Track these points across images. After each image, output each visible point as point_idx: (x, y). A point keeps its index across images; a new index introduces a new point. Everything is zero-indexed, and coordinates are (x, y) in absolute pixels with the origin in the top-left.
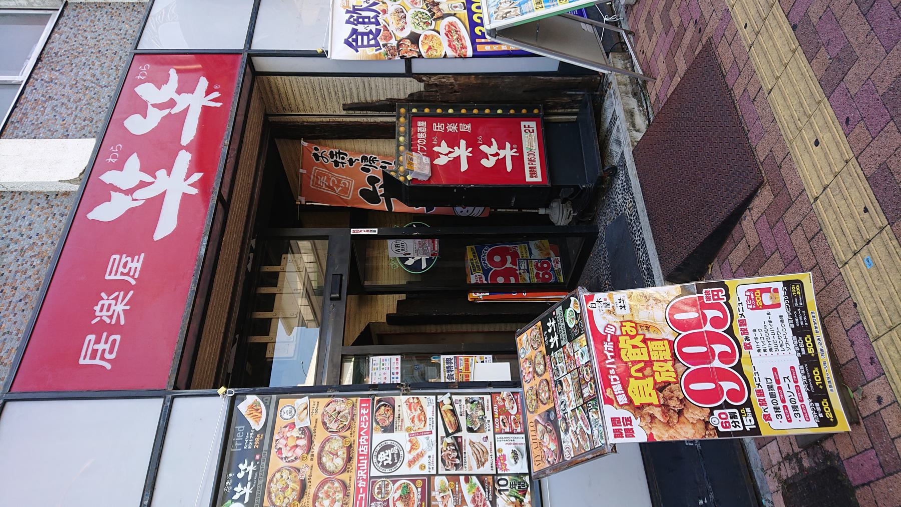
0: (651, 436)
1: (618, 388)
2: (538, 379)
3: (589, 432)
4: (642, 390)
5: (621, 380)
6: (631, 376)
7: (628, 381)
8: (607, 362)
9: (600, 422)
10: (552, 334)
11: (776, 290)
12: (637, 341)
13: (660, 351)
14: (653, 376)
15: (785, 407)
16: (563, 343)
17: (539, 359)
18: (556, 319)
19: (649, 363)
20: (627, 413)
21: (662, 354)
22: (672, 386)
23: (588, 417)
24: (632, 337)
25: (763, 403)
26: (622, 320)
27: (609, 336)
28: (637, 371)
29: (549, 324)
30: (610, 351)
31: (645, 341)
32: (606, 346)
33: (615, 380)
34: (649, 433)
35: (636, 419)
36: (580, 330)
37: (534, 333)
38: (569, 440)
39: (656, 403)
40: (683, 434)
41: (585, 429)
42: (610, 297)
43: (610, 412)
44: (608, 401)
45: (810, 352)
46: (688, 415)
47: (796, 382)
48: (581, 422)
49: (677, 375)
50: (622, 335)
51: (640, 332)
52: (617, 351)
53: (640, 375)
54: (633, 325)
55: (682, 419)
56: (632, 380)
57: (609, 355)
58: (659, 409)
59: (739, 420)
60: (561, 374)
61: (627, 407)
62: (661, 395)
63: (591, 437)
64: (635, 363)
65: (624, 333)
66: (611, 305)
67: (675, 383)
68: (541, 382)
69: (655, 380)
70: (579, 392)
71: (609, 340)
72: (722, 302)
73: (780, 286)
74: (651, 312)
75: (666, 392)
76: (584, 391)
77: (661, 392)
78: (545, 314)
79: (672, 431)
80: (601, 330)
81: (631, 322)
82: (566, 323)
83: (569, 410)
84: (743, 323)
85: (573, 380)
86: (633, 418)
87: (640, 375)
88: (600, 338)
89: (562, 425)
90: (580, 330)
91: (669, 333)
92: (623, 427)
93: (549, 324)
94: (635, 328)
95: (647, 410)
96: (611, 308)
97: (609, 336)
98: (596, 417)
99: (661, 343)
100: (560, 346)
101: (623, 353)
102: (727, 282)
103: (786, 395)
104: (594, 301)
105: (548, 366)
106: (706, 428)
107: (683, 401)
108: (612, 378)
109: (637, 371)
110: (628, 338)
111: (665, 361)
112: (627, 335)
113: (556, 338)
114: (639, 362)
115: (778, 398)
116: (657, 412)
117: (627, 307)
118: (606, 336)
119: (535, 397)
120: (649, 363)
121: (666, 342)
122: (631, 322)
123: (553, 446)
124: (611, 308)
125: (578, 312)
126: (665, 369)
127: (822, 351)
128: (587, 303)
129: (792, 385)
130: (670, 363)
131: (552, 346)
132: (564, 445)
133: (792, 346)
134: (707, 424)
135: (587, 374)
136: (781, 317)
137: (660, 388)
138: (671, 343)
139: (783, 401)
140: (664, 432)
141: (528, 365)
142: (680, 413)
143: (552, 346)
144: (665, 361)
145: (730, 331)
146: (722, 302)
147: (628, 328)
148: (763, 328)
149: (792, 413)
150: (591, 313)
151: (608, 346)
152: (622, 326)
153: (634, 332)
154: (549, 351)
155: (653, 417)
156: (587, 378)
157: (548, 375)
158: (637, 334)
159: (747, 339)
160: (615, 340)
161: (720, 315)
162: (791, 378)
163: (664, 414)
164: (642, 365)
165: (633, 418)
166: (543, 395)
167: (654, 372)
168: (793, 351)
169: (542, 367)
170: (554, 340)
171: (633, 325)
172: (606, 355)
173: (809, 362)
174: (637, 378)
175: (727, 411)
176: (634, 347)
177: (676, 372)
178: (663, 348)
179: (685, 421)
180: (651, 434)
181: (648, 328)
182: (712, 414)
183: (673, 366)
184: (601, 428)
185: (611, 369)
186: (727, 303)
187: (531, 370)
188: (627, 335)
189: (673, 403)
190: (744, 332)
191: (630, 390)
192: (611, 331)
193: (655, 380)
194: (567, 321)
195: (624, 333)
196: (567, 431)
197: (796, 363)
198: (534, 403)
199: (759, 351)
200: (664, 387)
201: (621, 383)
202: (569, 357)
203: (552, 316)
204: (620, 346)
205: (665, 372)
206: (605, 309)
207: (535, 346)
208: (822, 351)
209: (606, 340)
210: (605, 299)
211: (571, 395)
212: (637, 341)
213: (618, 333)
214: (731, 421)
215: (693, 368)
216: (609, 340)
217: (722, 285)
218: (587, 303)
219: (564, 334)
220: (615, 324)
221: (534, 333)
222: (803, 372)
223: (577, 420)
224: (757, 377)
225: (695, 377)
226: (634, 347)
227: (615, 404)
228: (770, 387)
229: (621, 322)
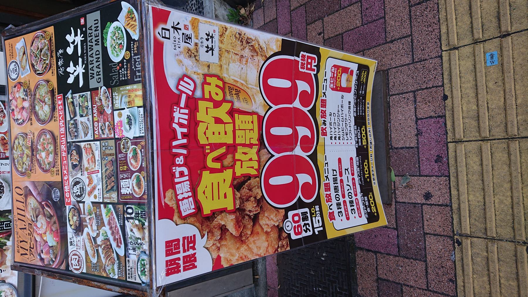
0: (217, 261)
1: (183, 188)
2: (37, 126)
3: (122, 253)
4: (216, 191)
5: (190, 175)
6: (206, 168)
7: (201, 175)
8: (175, 143)
9: (146, 247)
10: (74, 58)
11: (352, 72)
12: (222, 112)
13: (247, 131)
14: (233, 167)
15: (345, 202)
16: (93, 84)
17: (43, 91)
18: (84, 33)
19: (232, 148)
20: (190, 230)
21: (249, 135)
22: (253, 181)
23: (123, 228)
24: (217, 104)
25: (329, 199)
26: (206, 71)
27: (184, 96)
28: (215, 160)
29: (69, 38)
30: (181, 125)
31: (232, 112)
32: (176, 115)
33: (182, 174)
34: (215, 256)
35: (202, 237)
36: (133, 73)
37: (39, 44)
38: (81, 244)
39: (231, 207)
40: (255, 250)
41: (114, 245)
42: (195, 25)
43: (167, 230)
44: (167, 213)
45: (364, 144)
46: (263, 221)
47: (353, 174)
48: (107, 228)
49: (259, 165)
50: (203, 99)
51: (228, 98)
52: (193, 123)
53: (218, 165)
54: (220, 84)
55: (257, 228)
56: (206, 174)
57: (180, 131)
58: (233, 217)
59: (309, 222)
60: (82, 137)
61: (192, 219)
62: (238, 195)
63: (123, 261)
64: (215, 147)
65: (207, 96)
66: (194, 40)
67: (255, 176)
68: (42, 132)
69: (234, 173)
70: (113, 180)
71: (182, 104)
72: (312, 73)
73: (354, 67)
74: (245, 67)
75: (245, 191)
76: (123, 183)
77: (238, 190)
78: (65, 16)
79: (243, 248)
80: (172, 83)
81: (219, 78)
82: (105, 49)
83: (88, 200)
84: (324, 103)
85: (103, 155)
86: (198, 236)
87: (218, 165)
88: (168, 99)
89: (72, 220)
90: (133, 73)
91: (259, 104)
92: (181, 255)
93: (69, 38)
94: (223, 89)
95: (220, 220)
96: (192, 47)
97: (184, 96)
98: (138, 234)
99: (249, 118)
100: (86, 87)
101: (201, 129)
102: (323, 50)
103: (346, 188)
104: (169, 26)
105: (59, 112)
106: (280, 238)
107: (260, 202)
108: (177, 170)
109: (215, 160)
110: (211, 104)
111: (251, 146)
112: (211, 99)
113: (80, 70)
114: (220, 145)
115: (340, 193)
116: (229, 221)
117: (216, 51)
118: (180, 97)
119: (28, 152)
120: (232, 148)
121: (255, 117)
122: (219, 78)
123: (51, 240)
124: (192, 47)
125: (135, 36)
126: (247, 157)
127: (371, 142)
128: (155, 25)
129: (350, 177)
130: (255, 149)
131: (70, 80)
132: (70, 249)
133: (353, 136)
134: (280, 230)
135: (135, 157)
136: (350, 102)
137: (238, 184)
138: (261, 119)
139: (344, 196)
140: (234, 251)
141: (21, 94)
142: (255, 219)
143: (70, 80)
144: (251, 146)
145: (313, 112)
146: (312, 73)
147: (213, 89)
148: (336, 113)
149: (349, 208)
150: (159, 47)
151: (180, 115)
152: (205, 83)
153: (219, 98)
154: (64, 87)
155: (223, 230)
156: (134, 165)
157: (57, 127)
158: (224, 100)
159: (324, 123)
160: (192, 104)
161: (309, 90)
162: (349, 170)
163: (238, 223)
164: (223, 150)
165: (198, 236)
166: (43, 154)
167: (235, 161)
168: (354, 142)
169: (47, 109)
170: (76, 71)
171: (220, 84)
172: (174, 131)
173: (362, 152)
174: (213, 171)
175: (300, 211)
176: (218, 121)
177: (259, 161)
178: (250, 126)
179: (259, 230)
180: (219, 257)
181: (238, 92)
182: (286, 217)
183: (258, 153)
184: (145, 257)
185: (178, 155)
186: (316, 76)
187: (26, 104)
188: (211, 99)
189: (250, 206)
190: (324, 115)
191: (200, 190)
192: (187, 88)
193: (234, 173)
194: (108, 44)
195: (207, 96)
196: (79, 229)
197: (354, 154)
198: (26, 160)
199: (331, 138)
200: (244, 183)
201: (190, 180)
202: (101, 112)
203: (75, 24)
204: (200, 116)
205: (247, 163)
206: (183, 45)
207: (39, 67)
208: (371, 142)
209: (178, 104)
210: (186, 28)
211: (96, 178)
212: (222, 112)
213: (198, 94)
214: (302, 223)
215: (277, 156)
216: (182, 104)
217: (316, 51)
218: (155, 25)
219: (97, 67)
220: (195, 77)
221: (39, 44)
222: (358, 164)
223: (100, 224)
224: (326, 168)
225: (278, 168)
226: (218, 121)
227: (176, 217)
228: (335, 180)
229: (205, 76)
